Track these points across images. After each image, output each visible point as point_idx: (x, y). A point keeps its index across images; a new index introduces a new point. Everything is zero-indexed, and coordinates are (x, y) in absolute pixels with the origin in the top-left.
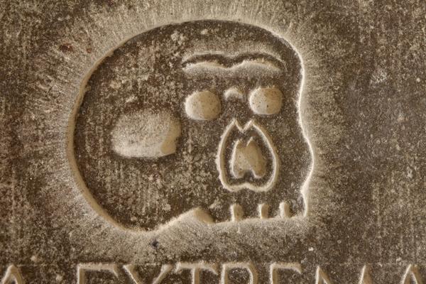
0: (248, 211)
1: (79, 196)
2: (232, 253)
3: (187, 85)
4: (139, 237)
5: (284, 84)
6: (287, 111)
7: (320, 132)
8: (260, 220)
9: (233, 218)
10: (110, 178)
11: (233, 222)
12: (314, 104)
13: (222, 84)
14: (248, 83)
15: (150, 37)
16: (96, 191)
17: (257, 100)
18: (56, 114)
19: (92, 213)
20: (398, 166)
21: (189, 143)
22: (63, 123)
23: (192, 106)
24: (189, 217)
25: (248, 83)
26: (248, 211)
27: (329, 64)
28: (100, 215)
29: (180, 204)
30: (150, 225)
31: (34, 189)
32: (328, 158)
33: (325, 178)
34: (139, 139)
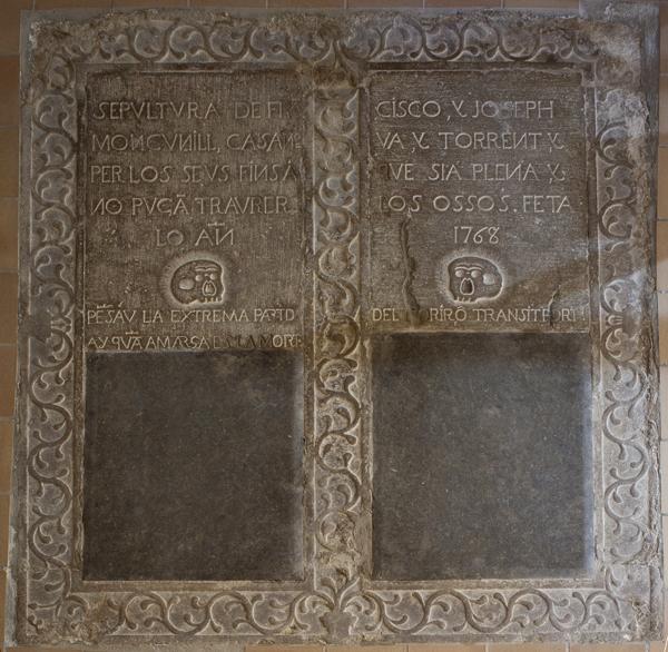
0: (209, 300)
1: (172, 297)
2: (272, 33)
3: (196, 274)
4: (185, 306)
5: (218, 273)
6: (219, 279)
7: (226, 284)
8: (212, 302)
9: (352, 276)
10: (179, 293)
11: (206, 303)
12: (225, 278)
13: (204, 273)
14: (210, 273)
15: (187, 264)
16: (175, 296)
17: (212, 277)
18: (167, 281)
19: (175, 301)
20: (243, 290)
21: (198, 286)
22: (169, 283)
23: (197, 278)
24: (196, 302)
25: (210, 273)
26: (209, 300)
27: (229, 269)
28: (552, 319)
29: (194, 299)
30: (187, 303)
31: (162, 296)
32: (228, 289)
33: (227, 293)
34: (185, 285)
